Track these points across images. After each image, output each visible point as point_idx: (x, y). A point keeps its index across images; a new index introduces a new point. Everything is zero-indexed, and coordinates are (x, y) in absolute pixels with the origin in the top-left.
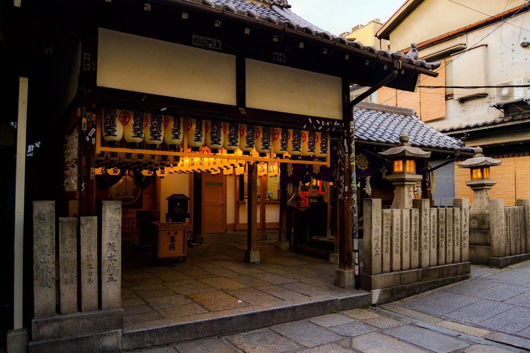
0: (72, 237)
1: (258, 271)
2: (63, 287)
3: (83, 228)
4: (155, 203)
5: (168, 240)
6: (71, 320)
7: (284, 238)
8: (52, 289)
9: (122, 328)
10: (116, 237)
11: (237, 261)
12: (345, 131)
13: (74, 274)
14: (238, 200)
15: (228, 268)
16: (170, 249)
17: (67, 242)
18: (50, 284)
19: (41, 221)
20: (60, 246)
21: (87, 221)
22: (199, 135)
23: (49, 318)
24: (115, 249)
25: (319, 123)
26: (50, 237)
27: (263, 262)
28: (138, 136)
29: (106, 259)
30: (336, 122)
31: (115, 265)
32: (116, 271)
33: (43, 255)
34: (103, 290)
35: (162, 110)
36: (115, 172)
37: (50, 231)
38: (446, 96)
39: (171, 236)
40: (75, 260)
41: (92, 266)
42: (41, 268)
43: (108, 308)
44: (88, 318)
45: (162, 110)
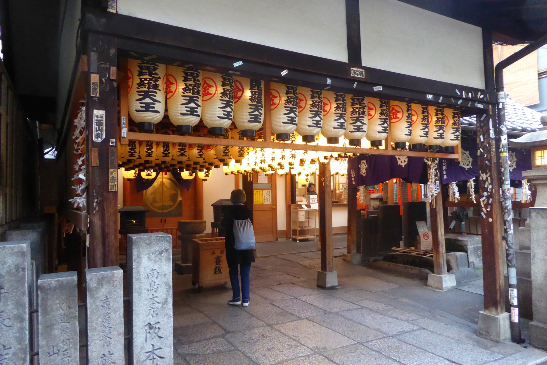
0: (68, 317)
1: (347, 305)
3: (92, 296)
4: (197, 212)
5: (222, 264)
7: (354, 251)
10: (163, 308)
11: (306, 285)
12: (490, 106)
14: (290, 203)
15: (304, 299)
16: (215, 273)
17: (56, 332)
21: (100, 282)
24: (160, 334)
25: (459, 93)
26: (17, 325)
27: (341, 285)
28: (192, 112)
29: (143, 357)
30: (479, 93)
35: (236, 64)
36: (149, 175)
37: (15, 312)
38: (539, 74)
39: (215, 256)
45: (236, 64)
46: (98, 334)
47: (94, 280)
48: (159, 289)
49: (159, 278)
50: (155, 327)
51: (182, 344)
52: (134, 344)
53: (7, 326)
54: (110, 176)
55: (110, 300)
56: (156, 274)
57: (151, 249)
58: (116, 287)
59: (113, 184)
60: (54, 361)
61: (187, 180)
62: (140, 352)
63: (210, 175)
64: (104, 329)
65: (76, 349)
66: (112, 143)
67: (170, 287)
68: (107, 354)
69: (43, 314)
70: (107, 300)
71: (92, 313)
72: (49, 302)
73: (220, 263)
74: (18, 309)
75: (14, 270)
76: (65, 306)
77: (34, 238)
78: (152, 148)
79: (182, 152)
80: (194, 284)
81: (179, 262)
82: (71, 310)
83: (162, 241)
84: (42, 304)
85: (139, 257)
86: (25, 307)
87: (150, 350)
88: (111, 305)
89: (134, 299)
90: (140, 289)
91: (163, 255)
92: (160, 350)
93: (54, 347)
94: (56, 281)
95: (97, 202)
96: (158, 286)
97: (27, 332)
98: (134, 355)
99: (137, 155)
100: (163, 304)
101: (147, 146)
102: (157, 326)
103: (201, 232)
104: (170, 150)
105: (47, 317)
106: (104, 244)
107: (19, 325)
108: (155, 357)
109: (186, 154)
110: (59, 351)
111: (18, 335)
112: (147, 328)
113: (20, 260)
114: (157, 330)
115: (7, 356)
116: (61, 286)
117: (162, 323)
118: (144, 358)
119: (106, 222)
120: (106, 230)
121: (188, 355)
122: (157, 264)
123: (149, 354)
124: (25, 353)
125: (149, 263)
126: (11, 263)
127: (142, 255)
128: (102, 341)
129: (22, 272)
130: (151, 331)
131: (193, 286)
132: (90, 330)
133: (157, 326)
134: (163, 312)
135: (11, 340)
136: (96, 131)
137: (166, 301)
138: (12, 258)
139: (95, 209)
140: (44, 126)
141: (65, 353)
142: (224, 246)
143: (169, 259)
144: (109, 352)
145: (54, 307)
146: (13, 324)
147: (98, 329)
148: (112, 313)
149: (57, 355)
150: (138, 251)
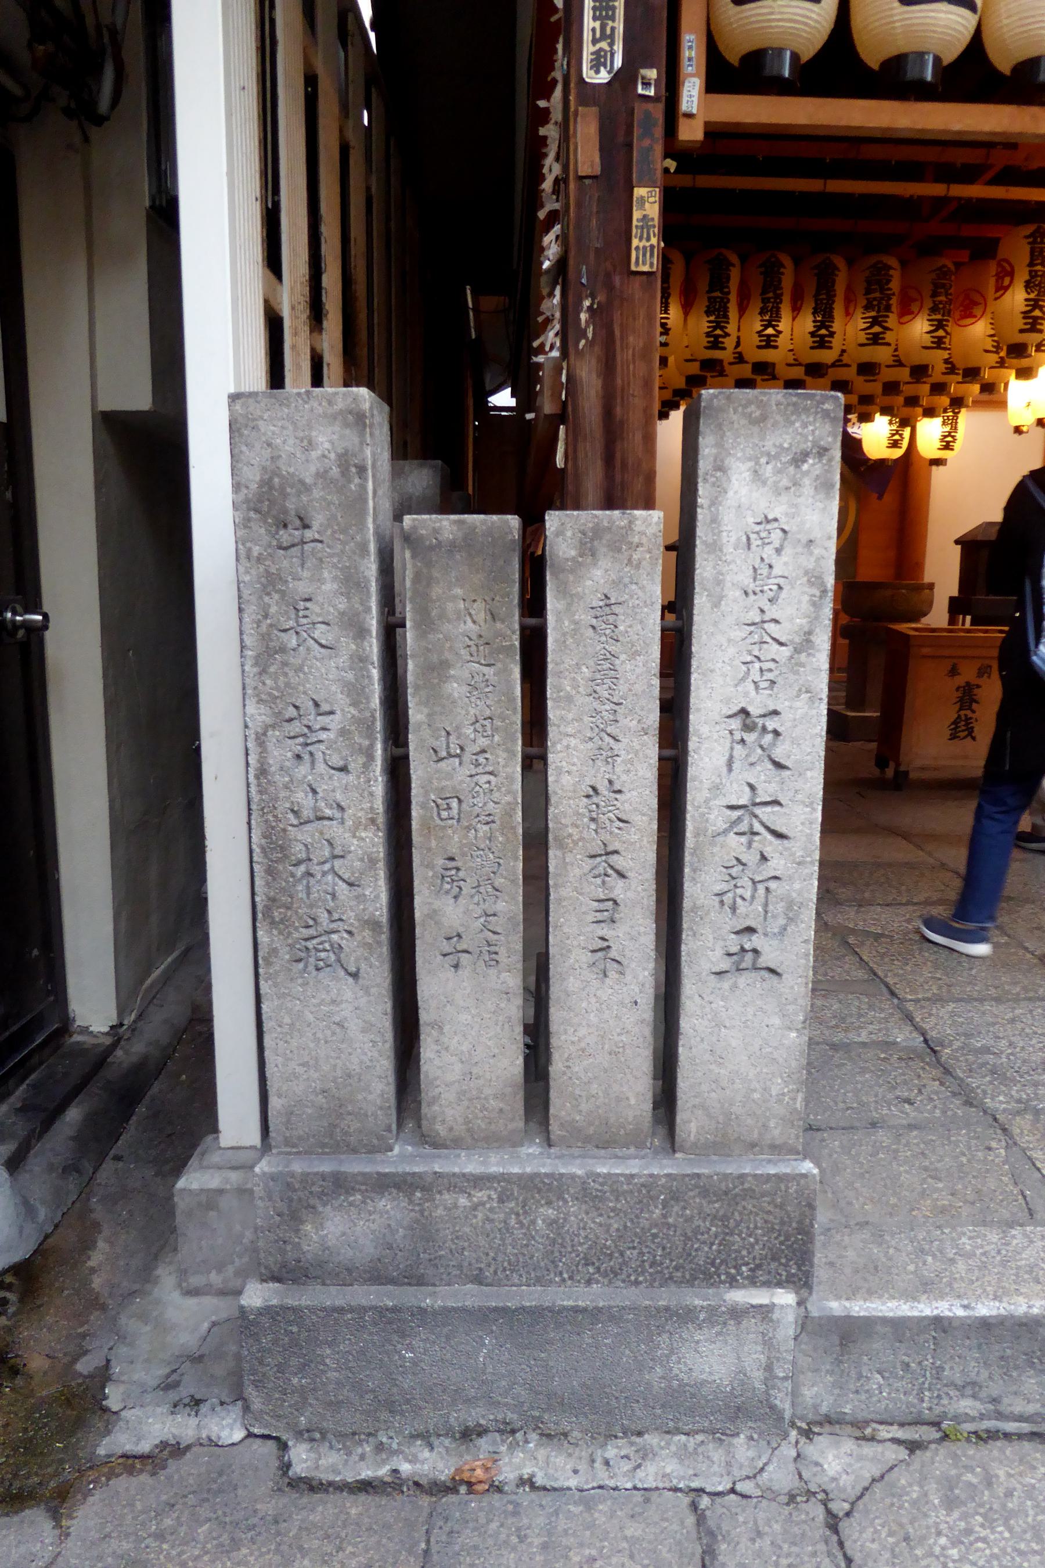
2: (433, 984)
3: (563, 591)
6: (480, 1195)
8: (367, 990)
9: (801, 1281)
13: (501, 906)
16: (953, 737)
17: (455, 689)
18: (353, 950)
19: (285, 537)
20: (416, 714)
21: (589, 545)
22: (823, 332)
23: (355, 1166)
24: (778, 754)
26: (347, 645)
29: (718, 819)
31: (777, 864)
32: (778, 908)
33: (303, 769)
34: (692, 1021)
37: (342, 604)
39: (960, 681)
40: (509, 814)
41: (616, 860)
42: (298, 850)
43: (720, 1146)
44: (591, 1194)
46: (579, 720)
47: (569, 534)
48: (784, 594)
49: (788, 551)
50: (764, 729)
51: (838, 903)
52: (691, 771)
53: (323, 646)
54: (637, 215)
55: (616, 609)
56: (776, 536)
57: (763, 439)
58: (638, 567)
59: (644, 243)
60: (449, 776)
61: (882, 462)
62: (707, 801)
63: (957, 446)
64: (596, 704)
65: (512, 753)
66: (646, 84)
67: (824, 592)
68: (603, 788)
69: (417, 626)
70: (607, 610)
71: (562, 643)
72: (436, 591)
73: (974, 706)
74: (349, 598)
75: (335, 471)
76: (479, 610)
77: (425, 484)
78: (778, 318)
79: (877, 329)
80: (881, 762)
81: (839, 708)
82: (499, 625)
83: (806, 410)
84: (415, 592)
85: (720, 467)
86: (369, 597)
87: (741, 802)
88: (621, 628)
89: (696, 618)
90: (719, 583)
91: (805, 467)
92: (777, 808)
93: (448, 733)
94: (455, 522)
95: (590, 308)
96: (781, 581)
97: (375, 673)
98: (689, 807)
99: (729, 343)
100: (797, 651)
101: (762, 313)
102: (771, 724)
103: (916, 615)
104: (836, 326)
105: (431, 636)
106: (609, 459)
107: (354, 647)
108: (757, 827)
109: (889, 337)
110: (462, 749)
111: (350, 676)
112: (736, 724)
113: (351, 439)
114: (769, 737)
115: (323, 736)
116: (468, 544)
117: (787, 716)
118: (722, 825)
119: (619, 381)
120: (618, 410)
121: (853, 931)
122: (784, 498)
123: (737, 813)
124: (371, 737)
125: (755, 495)
126: (327, 445)
127: (730, 462)
128: (590, 745)
129: (357, 480)
130: (751, 737)
131: (877, 772)
132: (554, 700)
133: (771, 724)
134: (792, 677)
135: (333, 688)
136: (595, 41)
137: (808, 641)
138: (329, 430)
139: (584, 334)
140: (490, 302)
141: (481, 760)
142: (995, 653)
143: (828, 486)
144: (610, 782)
145: (450, 606)
146: (338, 641)
147: (580, 700)
148: (623, 657)
149: (457, 760)
150: (719, 445)
